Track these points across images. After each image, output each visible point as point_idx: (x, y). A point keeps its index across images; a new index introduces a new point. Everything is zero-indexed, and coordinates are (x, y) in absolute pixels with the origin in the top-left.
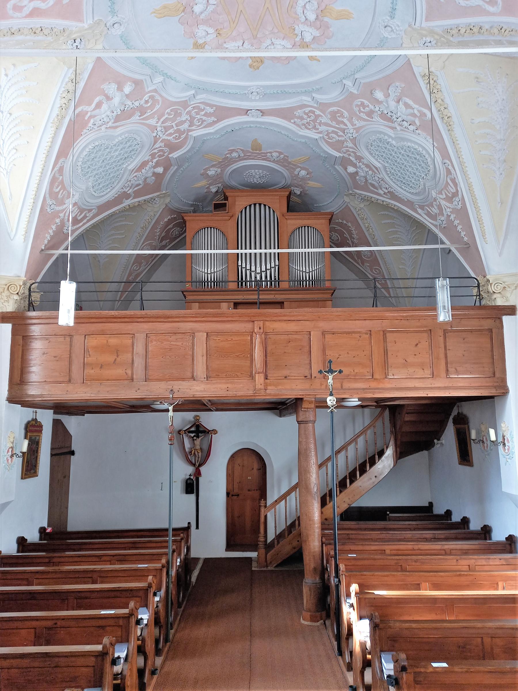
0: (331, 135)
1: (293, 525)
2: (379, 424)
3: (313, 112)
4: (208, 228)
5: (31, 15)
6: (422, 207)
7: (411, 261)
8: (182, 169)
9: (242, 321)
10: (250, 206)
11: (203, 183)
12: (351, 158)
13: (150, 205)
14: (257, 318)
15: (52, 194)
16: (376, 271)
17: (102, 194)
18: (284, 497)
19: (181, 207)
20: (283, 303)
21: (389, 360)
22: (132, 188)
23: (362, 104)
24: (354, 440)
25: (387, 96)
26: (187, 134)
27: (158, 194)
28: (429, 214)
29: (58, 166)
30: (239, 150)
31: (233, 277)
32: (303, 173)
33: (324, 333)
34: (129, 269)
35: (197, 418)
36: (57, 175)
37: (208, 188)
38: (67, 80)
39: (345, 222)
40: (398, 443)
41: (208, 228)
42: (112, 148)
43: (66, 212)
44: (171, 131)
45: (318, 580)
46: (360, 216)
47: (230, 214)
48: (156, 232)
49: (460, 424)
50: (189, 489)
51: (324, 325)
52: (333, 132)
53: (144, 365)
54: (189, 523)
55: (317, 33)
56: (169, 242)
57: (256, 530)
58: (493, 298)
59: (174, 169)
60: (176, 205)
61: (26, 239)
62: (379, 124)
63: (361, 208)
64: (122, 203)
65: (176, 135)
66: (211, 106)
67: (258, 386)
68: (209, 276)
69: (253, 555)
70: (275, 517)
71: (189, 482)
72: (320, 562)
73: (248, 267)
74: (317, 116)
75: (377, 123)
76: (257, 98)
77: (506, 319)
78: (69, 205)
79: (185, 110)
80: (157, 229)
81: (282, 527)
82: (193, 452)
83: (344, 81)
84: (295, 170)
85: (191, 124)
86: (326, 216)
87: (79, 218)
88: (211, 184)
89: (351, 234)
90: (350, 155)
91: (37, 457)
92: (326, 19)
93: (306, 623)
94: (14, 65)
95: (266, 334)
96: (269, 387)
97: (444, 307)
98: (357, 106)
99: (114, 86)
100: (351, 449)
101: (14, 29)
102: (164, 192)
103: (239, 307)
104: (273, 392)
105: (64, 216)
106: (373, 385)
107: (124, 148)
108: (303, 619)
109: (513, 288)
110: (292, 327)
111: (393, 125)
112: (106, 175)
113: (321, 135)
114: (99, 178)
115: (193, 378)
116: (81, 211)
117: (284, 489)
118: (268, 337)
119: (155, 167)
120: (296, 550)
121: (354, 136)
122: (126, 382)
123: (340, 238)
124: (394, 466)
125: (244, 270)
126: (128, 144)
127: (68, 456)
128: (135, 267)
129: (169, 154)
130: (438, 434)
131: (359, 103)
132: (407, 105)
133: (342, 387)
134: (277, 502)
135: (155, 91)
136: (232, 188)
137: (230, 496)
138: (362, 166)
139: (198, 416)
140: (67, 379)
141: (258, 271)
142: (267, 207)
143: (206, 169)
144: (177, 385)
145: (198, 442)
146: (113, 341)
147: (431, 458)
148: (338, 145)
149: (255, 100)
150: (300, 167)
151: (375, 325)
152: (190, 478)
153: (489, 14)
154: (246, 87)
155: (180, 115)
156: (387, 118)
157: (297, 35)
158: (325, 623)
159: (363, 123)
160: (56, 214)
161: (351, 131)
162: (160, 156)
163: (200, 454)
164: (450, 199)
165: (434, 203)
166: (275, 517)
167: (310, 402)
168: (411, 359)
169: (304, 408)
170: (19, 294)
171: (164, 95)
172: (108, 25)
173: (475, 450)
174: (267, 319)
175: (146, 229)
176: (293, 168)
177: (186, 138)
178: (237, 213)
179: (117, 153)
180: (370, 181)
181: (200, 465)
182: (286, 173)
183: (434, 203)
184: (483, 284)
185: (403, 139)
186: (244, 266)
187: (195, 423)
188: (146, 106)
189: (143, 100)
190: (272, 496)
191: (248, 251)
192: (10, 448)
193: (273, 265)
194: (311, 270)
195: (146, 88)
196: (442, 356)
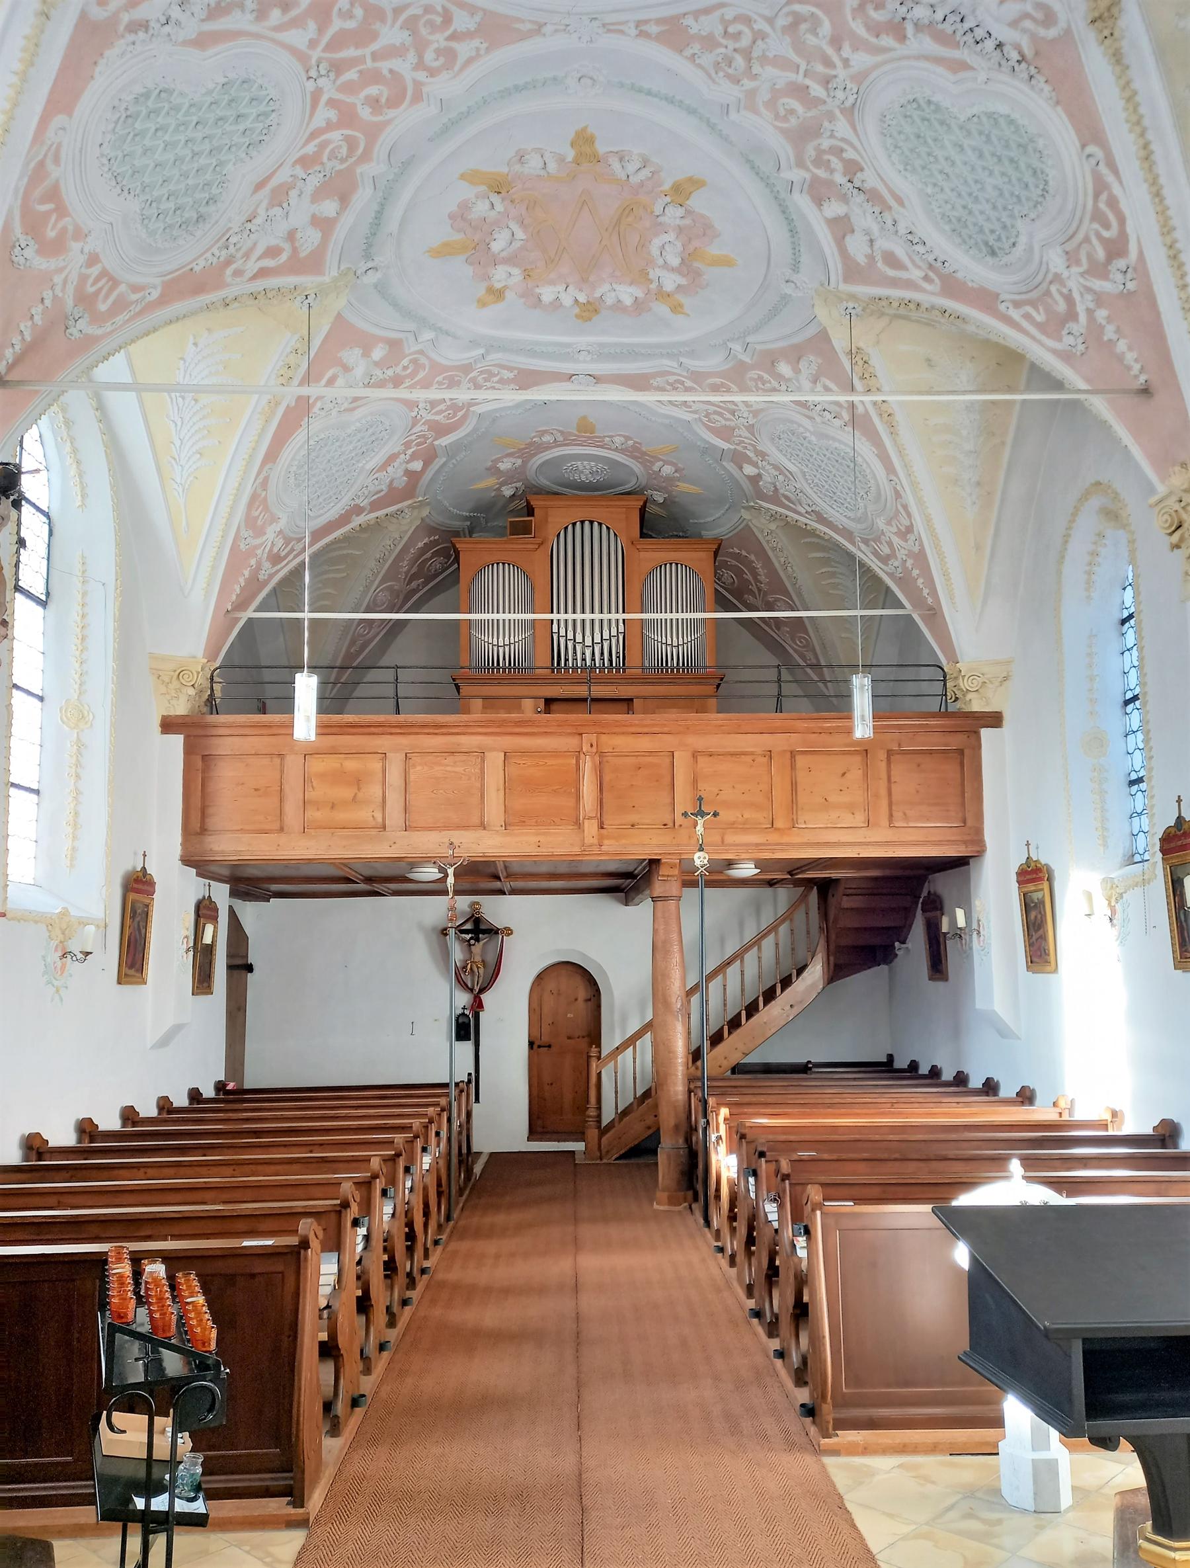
0: (712, 416)
1: (647, 1094)
2: (800, 915)
4: (498, 564)
5: (254, 277)
6: (866, 542)
8: (454, 461)
9: (560, 734)
10: (574, 524)
11: (491, 481)
12: (748, 452)
13: (394, 520)
15: (250, 521)
16: (801, 642)
17: (321, 512)
18: (631, 1041)
19: (449, 522)
20: (631, 700)
21: (799, 798)
23: (760, 378)
24: (757, 942)
25: (797, 371)
26: (468, 410)
27: (410, 502)
28: (876, 553)
29: (262, 476)
30: (554, 432)
31: (543, 659)
32: (667, 470)
33: (695, 755)
34: (351, 633)
35: (475, 910)
36: (259, 491)
37: (498, 489)
38: (289, 349)
39: (744, 553)
40: (832, 947)
41: (498, 564)
42: (344, 439)
44: (442, 407)
45: (681, 1141)
47: (539, 540)
48: (402, 567)
50: (462, 1032)
51: (697, 742)
52: (715, 412)
53: (403, 804)
55: (683, 281)
56: (423, 582)
57: (581, 1105)
58: (967, 699)
59: (442, 462)
60: (439, 519)
63: (772, 532)
64: (349, 522)
66: (510, 369)
67: (589, 840)
68: (501, 650)
69: (578, 1146)
70: (616, 1083)
71: (460, 1021)
72: (683, 1116)
73: (570, 636)
76: (588, 359)
77: (985, 732)
78: (271, 533)
80: (403, 561)
81: (627, 1099)
82: (469, 966)
83: (730, 345)
84: (653, 463)
86: (710, 546)
87: (283, 554)
88: (502, 484)
89: (755, 574)
92: (696, 264)
93: (662, 1208)
94: (208, 330)
95: (601, 754)
96: (606, 842)
97: (863, 718)
98: (751, 379)
99: (358, 351)
100: (750, 957)
101: (230, 298)
102: (420, 499)
103: (554, 707)
104: (611, 849)
106: (773, 837)
107: (363, 438)
108: (657, 1204)
109: (997, 684)
110: (645, 743)
111: (810, 413)
112: (329, 482)
113: (697, 416)
114: (320, 488)
115: (483, 826)
116: (287, 541)
117: (634, 1027)
118: (605, 759)
119: (408, 462)
120: (650, 1132)
122: (374, 832)
124: (824, 988)
125: (562, 641)
126: (370, 431)
127: (243, 972)
129: (436, 439)
130: (900, 933)
131: (756, 377)
133: (723, 841)
134: (619, 1049)
135: (421, 352)
136: (540, 491)
137: (535, 1047)
138: (768, 467)
139: (478, 903)
140: (276, 826)
141: (588, 642)
142: (604, 527)
144: (458, 837)
145: (477, 948)
146: (351, 765)
148: (725, 433)
149: (585, 362)
151: (778, 742)
152: (463, 1014)
153: (924, 291)
154: (568, 345)
157: (651, 281)
158: (690, 1208)
160: (251, 552)
162: (418, 445)
163: (481, 971)
165: (883, 537)
166: (616, 1083)
168: (834, 798)
169: (663, 876)
170: (196, 686)
171: (434, 356)
172: (359, 273)
174: (604, 731)
175: (385, 561)
176: (649, 461)
177: (465, 417)
178: (551, 537)
179: (351, 447)
181: (482, 991)
183: (883, 537)
185: (827, 437)
186: (562, 633)
187: (473, 915)
188: (404, 373)
189: (401, 366)
190: (611, 1042)
191: (570, 616)
193: (614, 632)
194: (681, 643)
196: (883, 792)
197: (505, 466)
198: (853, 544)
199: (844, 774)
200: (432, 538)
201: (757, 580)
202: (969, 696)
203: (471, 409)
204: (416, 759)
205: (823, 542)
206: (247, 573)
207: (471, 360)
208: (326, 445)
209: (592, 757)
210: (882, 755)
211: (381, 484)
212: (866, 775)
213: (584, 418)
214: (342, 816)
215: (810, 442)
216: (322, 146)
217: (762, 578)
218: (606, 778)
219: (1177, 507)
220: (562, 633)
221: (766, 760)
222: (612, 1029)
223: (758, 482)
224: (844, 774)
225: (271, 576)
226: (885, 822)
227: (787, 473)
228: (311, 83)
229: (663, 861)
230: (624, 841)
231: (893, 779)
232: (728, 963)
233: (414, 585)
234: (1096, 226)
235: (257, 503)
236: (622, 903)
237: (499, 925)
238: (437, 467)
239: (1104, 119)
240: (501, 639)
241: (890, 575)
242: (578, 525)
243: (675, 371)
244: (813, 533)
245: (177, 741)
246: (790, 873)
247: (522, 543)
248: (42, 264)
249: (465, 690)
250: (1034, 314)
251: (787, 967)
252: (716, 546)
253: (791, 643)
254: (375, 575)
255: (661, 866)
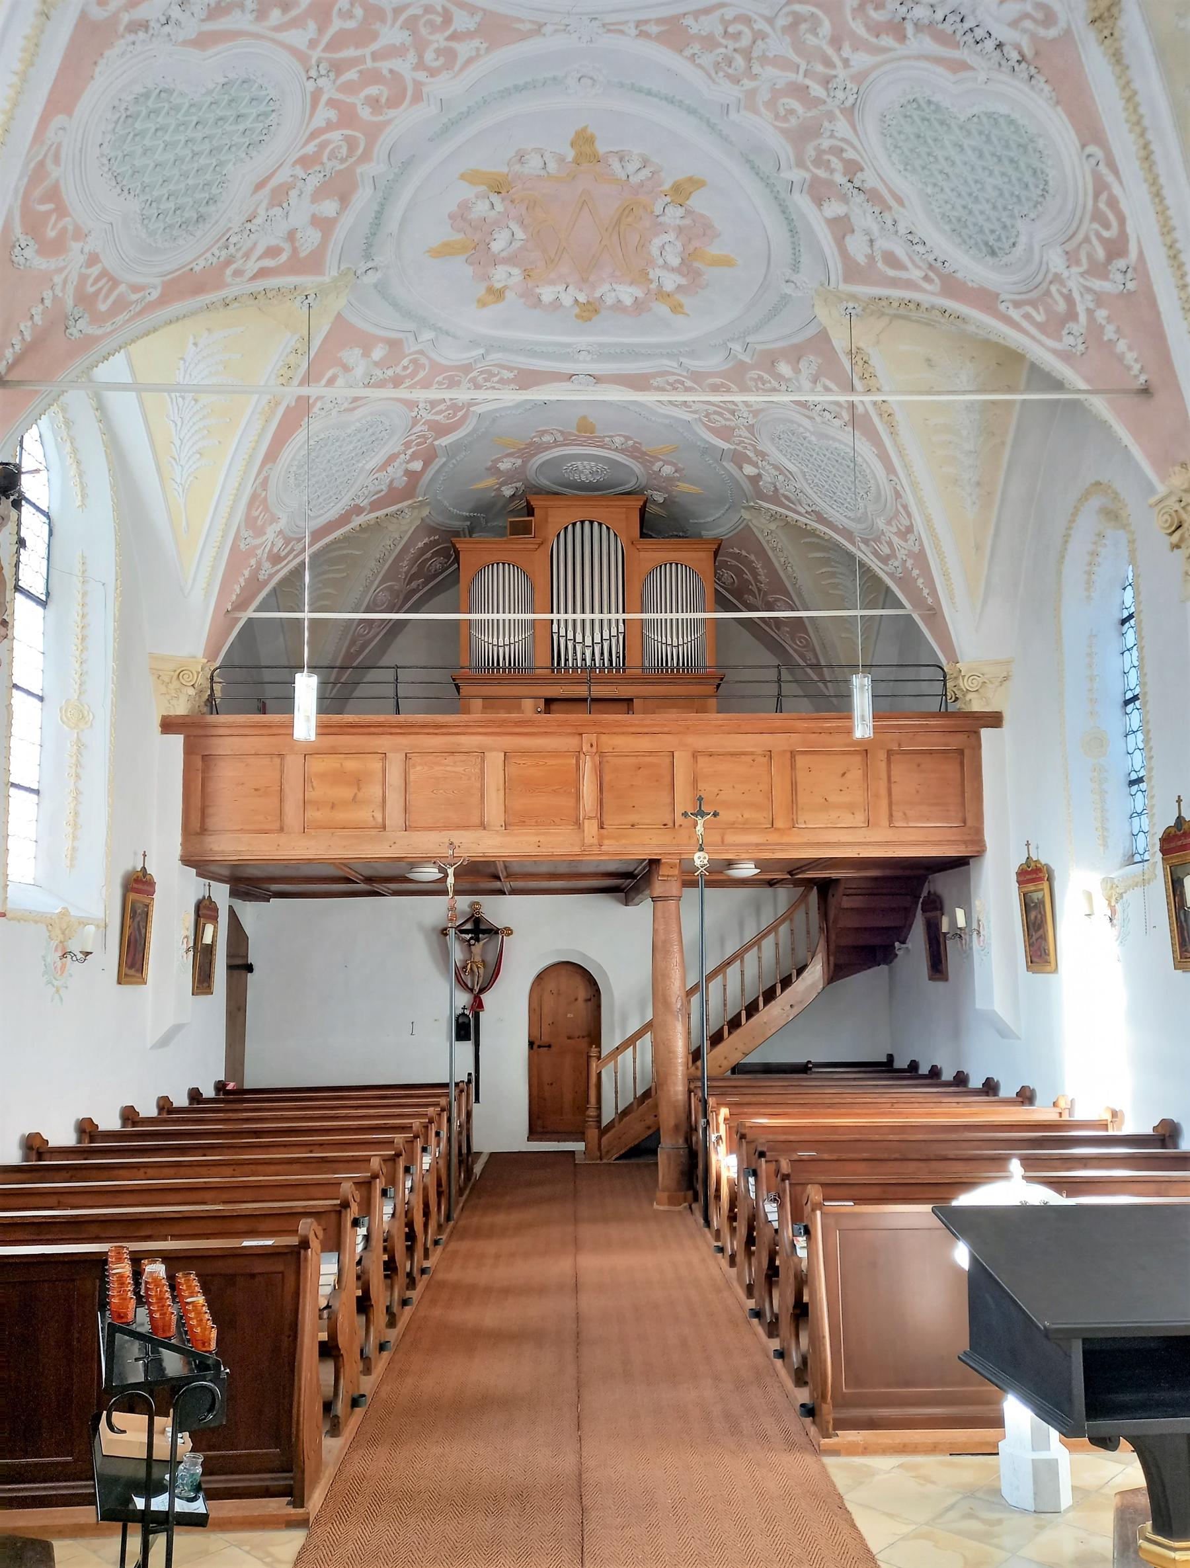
0: (712, 416)
1: (647, 1094)
2: (800, 915)
4: (498, 564)
5: (254, 277)
6: (866, 542)
8: (454, 461)
9: (560, 734)
10: (574, 524)
11: (491, 481)
12: (748, 452)
13: (394, 520)
15: (250, 521)
16: (801, 642)
17: (321, 512)
18: (631, 1041)
19: (449, 522)
20: (631, 700)
21: (799, 798)
23: (760, 378)
24: (757, 942)
25: (797, 371)
26: (468, 410)
27: (410, 502)
28: (876, 553)
29: (262, 476)
30: (554, 432)
31: (543, 659)
32: (667, 470)
33: (695, 755)
34: (351, 633)
35: (475, 910)
36: (259, 491)
37: (498, 489)
38: (289, 349)
39: (744, 553)
40: (832, 947)
41: (498, 564)
42: (344, 439)
44: (442, 407)
45: (681, 1141)
47: (539, 540)
48: (402, 567)
50: (462, 1032)
51: (697, 742)
52: (715, 412)
53: (403, 804)
55: (683, 281)
56: (423, 582)
57: (581, 1105)
58: (967, 699)
59: (442, 462)
60: (439, 519)
63: (772, 532)
64: (349, 522)
66: (510, 369)
67: (589, 840)
68: (501, 650)
69: (578, 1146)
70: (616, 1083)
71: (460, 1021)
72: (683, 1116)
73: (570, 636)
76: (588, 359)
77: (985, 732)
78: (271, 533)
80: (403, 561)
81: (627, 1099)
82: (469, 966)
83: (730, 345)
84: (653, 463)
86: (710, 546)
87: (283, 554)
88: (502, 484)
89: (755, 574)
92: (696, 264)
93: (662, 1208)
94: (208, 330)
95: (601, 754)
96: (606, 842)
97: (863, 718)
98: (751, 379)
99: (358, 351)
100: (750, 957)
101: (230, 298)
102: (420, 499)
103: (554, 707)
104: (611, 849)
106: (773, 837)
107: (363, 438)
108: (657, 1204)
109: (997, 684)
110: (645, 743)
111: (810, 413)
112: (329, 482)
113: (697, 416)
114: (320, 488)
115: (483, 826)
116: (287, 541)
117: (634, 1027)
118: (605, 759)
119: (408, 462)
120: (650, 1132)
122: (374, 832)
124: (824, 988)
125: (562, 641)
126: (370, 431)
127: (243, 972)
129: (436, 439)
130: (900, 933)
131: (756, 377)
133: (723, 841)
134: (619, 1049)
135: (421, 352)
136: (540, 491)
137: (535, 1047)
138: (768, 467)
139: (478, 903)
140: (276, 826)
141: (588, 642)
142: (604, 527)
144: (458, 837)
145: (477, 948)
146: (351, 765)
148: (725, 433)
149: (585, 362)
151: (778, 742)
152: (463, 1014)
153: (924, 291)
154: (568, 345)
157: (651, 281)
158: (690, 1208)
160: (251, 552)
162: (418, 445)
163: (481, 971)
165: (883, 537)
166: (616, 1083)
168: (834, 798)
169: (663, 876)
170: (196, 686)
171: (434, 356)
172: (359, 273)
174: (604, 731)
175: (385, 561)
176: (649, 461)
177: (465, 417)
178: (551, 537)
179: (351, 447)
181: (482, 991)
183: (883, 537)
185: (827, 437)
186: (562, 633)
187: (473, 915)
188: (404, 373)
189: (401, 366)
190: (611, 1042)
191: (570, 616)
193: (614, 632)
194: (681, 643)
196: (883, 792)
197: (505, 466)
198: (853, 544)
199: (844, 774)
200: (432, 538)
201: (757, 580)
202: (969, 696)
203: (471, 409)
204: (416, 759)
205: (823, 542)
206: (247, 573)
207: (471, 360)
208: (326, 445)
209: (592, 757)
210: (882, 755)
211: (381, 484)
212: (866, 775)
213: (584, 418)
214: (342, 816)
215: (810, 442)
216: (322, 146)
217: (762, 578)
218: (606, 778)
219: (1177, 507)
220: (562, 633)
221: (766, 760)
222: (612, 1029)
223: (758, 482)
224: (844, 774)
225: (271, 576)
226: (885, 822)
227: (787, 473)
228: (311, 83)
229: (663, 861)
230: (624, 841)
231: (893, 779)
232: (728, 963)
233: (414, 585)
234: (1096, 226)
235: (257, 503)
236: (622, 903)
237: (499, 925)
238: (437, 467)
239: (1104, 119)
240: (501, 639)
241: (890, 575)
242: (578, 525)
243: (675, 371)
244: (813, 533)
245: (177, 741)
246: (790, 873)
247: (522, 543)
248: (42, 264)
249: (465, 690)
250: (1034, 314)
251: (787, 967)
252: (716, 546)
253: (791, 643)
254: (375, 575)
255: (661, 866)
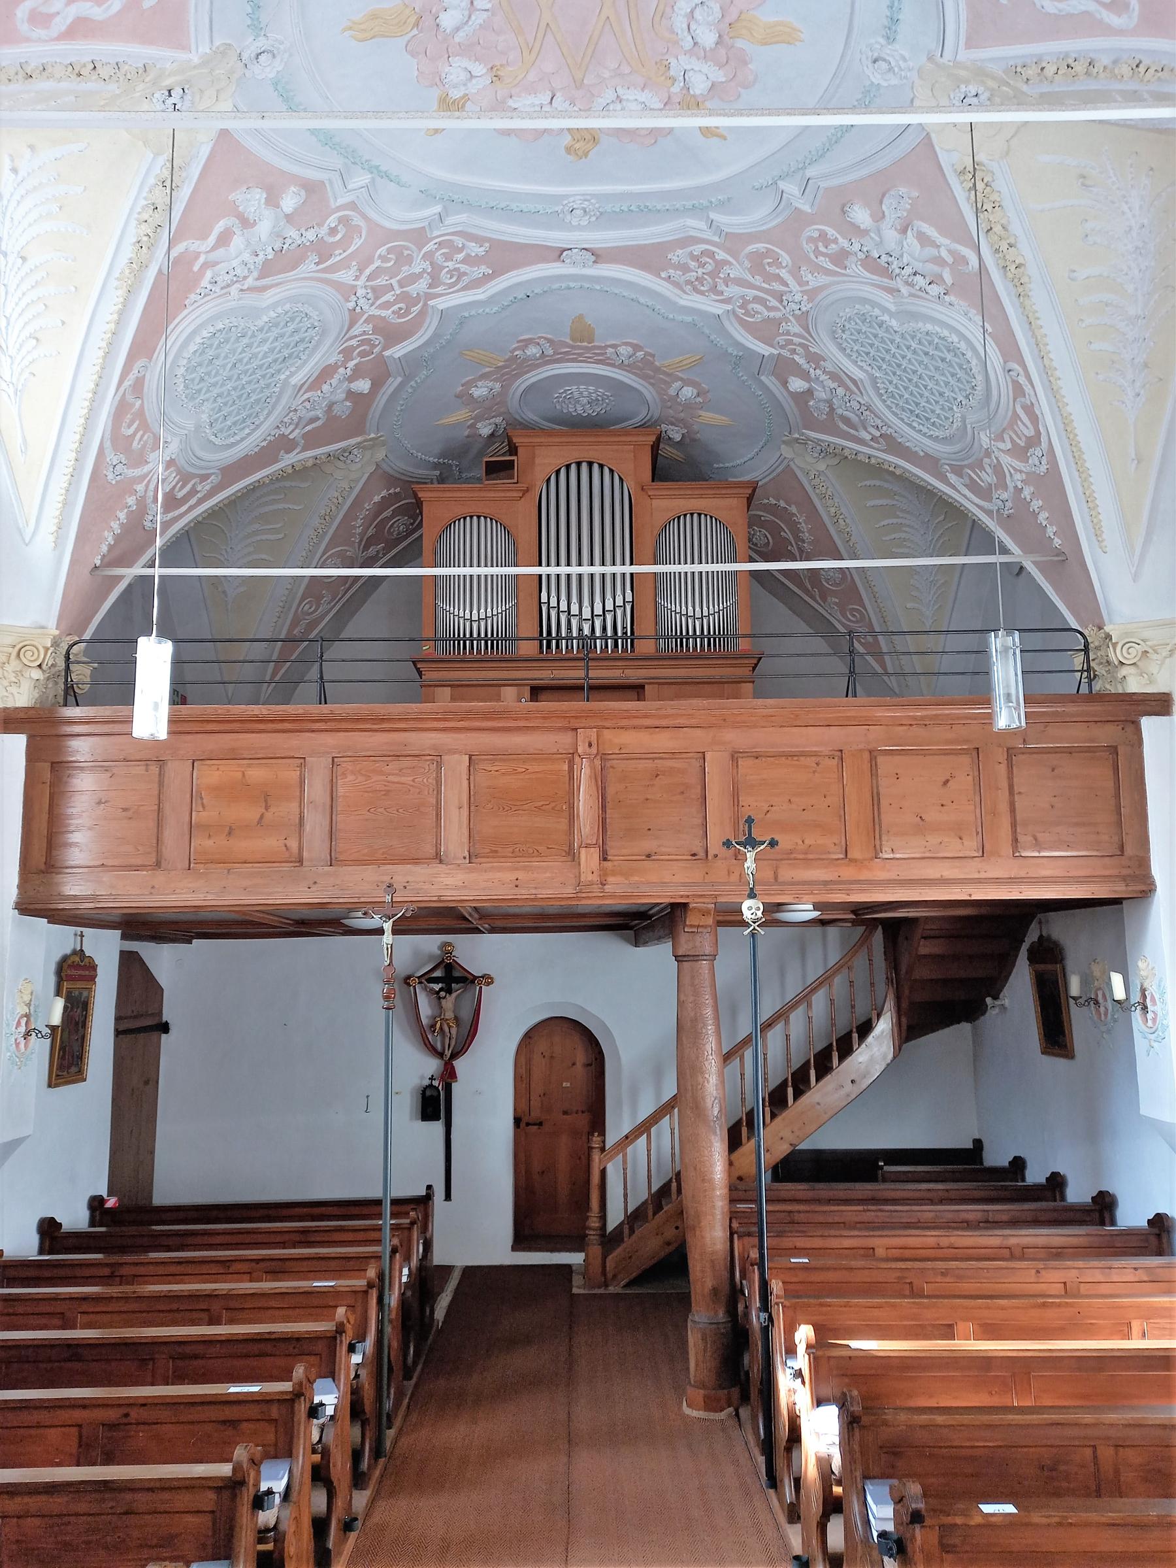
0: (751, 306)
1: (665, 1190)
2: (860, 961)
3: (711, 255)
4: (471, 517)
5: (70, 33)
6: (958, 471)
7: (932, 592)
8: (413, 383)
9: (549, 729)
10: (568, 467)
11: (461, 415)
12: (796, 357)
13: (340, 464)
14: (583, 723)
15: (118, 440)
16: (854, 616)
17: (232, 440)
18: (645, 1128)
19: (411, 470)
20: (642, 687)
21: (883, 816)
22: (301, 426)
23: (823, 236)
24: (804, 998)
25: (879, 217)
26: (425, 305)
27: (359, 439)
28: (973, 486)
29: (132, 377)
30: (542, 341)
31: (528, 628)
32: (688, 392)
33: (735, 756)
34: (293, 610)
35: (447, 949)
36: (130, 398)
37: (472, 426)
38: (152, 181)
39: (782, 504)
40: (904, 1005)
41: (471, 517)
42: (253, 336)
43: (149, 482)
44: (389, 297)
45: (721, 1315)
46: (817, 491)
47: (521, 486)
48: (354, 527)
49: (1043, 961)
50: (430, 1110)
51: (736, 738)
52: (756, 299)
53: (328, 828)
54: (429, 1187)
55: (719, 76)
56: (384, 549)
57: (580, 1202)
58: (1120, 676)
59: (396, 384)
60: (400, 465)
61: (58, 543)
62: (862, 282)
63: (820, 473)
64: (276, 461)
65: (399, 306)
66: (480, 240)
67: (586, 877)
68: (475, 625)
69: (575, 1258)
70: (625, 1174)
71: (428, 1093)
72: (726, 1274)
73: (563, 607)
74: (720, 264)
75: (855, 279)
76: (584, 223)
77: (1148, 725)
78: (157, 465)
79: (420, 250)
80: (355, 520)
81: (640, 1195)
82: (438, 1026)
83: (782, 185)
84: (669, 385)
85: (435, 282)
86: (741, 491)
87: (180, 495)
88: (478, 419)
89: (796, 531)
90: (794, 352)
91: (83, 1037)
92: (740, 43)
93: (695, 1413)
94: (32, 147)
95: (604, 757)
96: (611, 879)
97: (1008, 697)
98: (811, 239)
99: (259, 195)
100: (797, 1018)
101: (33, 65)
102: (372, 435)
103: (542, 696)
104: (619, 891)
105: (146, 491)
106: (848, 873)
107: (282, 336)
108: (689, 1406)
109: (1165, 653)
110: (663, 741)
111: (892, 284)
112: (240, 397)
113: (729, 307)
114: (225, 404)
115: (438, 858)
116: (185, 478)
117: (646, 1110)
118: (608, 764)
119: (351, 379)
120: (672, 1248)
121: (804, 309)
122: (286, 867)
123: (771, 541)
124: (894, 1058)
125: (553, 613)
126: (292, 327)
127: (154, 1035)
128: (307, 607)
129: (385, 349)
130: (994, 985)
131: (816, 235)
132: (923, 239)
133: (776, 878)
134: (629, 1139)
135: (353, 206)
136: (528, 427)
137: (523, 1125)
138: (823, 377)
139: (450, 944)
140: (152, 860)
141: (587, 614)
142: (606, 470)
143: (468, 384)
144: (401, 874)
145: (449, 1002)
146: (257, 774)
147: (977, 1040)
148: (767, 330)
149: (579, 228)
150: (681, 379)
151: (852, 738)
152: (431, 1086)
153: (1110, 31)
154: (558, 198)
155: (409, 260)
156: (878, 267)
157: (674, 80)
158: (737, 1415)
159: (823, 280)
160: (127, 487)
161: (798, 298)
162: (363, 354)
163: (454, 1031)
164: (1021, 452)
165: (986, 460)
166: (625, 1174)
167: (705, 913)
168: (932, 816)
169: (691, 926)
170: (44, 666)
171: (372, 215)
172: (245, 56)
173: (1079, 1021)
174: (607, 724)
175: (332, 519)
176: (665, 382)
177: (422, 314)
178: (539, 483)
179: (265, 348)
180: (840, 411)
181: (455, 1055)
182: (648, 392)
183: (986, 460)
184: (1097, 644)
185: (914, 316)
186: (553, 603)
187: (443, 961)
188: (331, 240)
189: (326, 227)
190: (618, 1125)
191: (563, 570)
192: (22, 1016)
193: (619, 602)
194: (705, 613)
195: (332, 201)
196: (1004, 807)
